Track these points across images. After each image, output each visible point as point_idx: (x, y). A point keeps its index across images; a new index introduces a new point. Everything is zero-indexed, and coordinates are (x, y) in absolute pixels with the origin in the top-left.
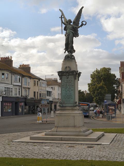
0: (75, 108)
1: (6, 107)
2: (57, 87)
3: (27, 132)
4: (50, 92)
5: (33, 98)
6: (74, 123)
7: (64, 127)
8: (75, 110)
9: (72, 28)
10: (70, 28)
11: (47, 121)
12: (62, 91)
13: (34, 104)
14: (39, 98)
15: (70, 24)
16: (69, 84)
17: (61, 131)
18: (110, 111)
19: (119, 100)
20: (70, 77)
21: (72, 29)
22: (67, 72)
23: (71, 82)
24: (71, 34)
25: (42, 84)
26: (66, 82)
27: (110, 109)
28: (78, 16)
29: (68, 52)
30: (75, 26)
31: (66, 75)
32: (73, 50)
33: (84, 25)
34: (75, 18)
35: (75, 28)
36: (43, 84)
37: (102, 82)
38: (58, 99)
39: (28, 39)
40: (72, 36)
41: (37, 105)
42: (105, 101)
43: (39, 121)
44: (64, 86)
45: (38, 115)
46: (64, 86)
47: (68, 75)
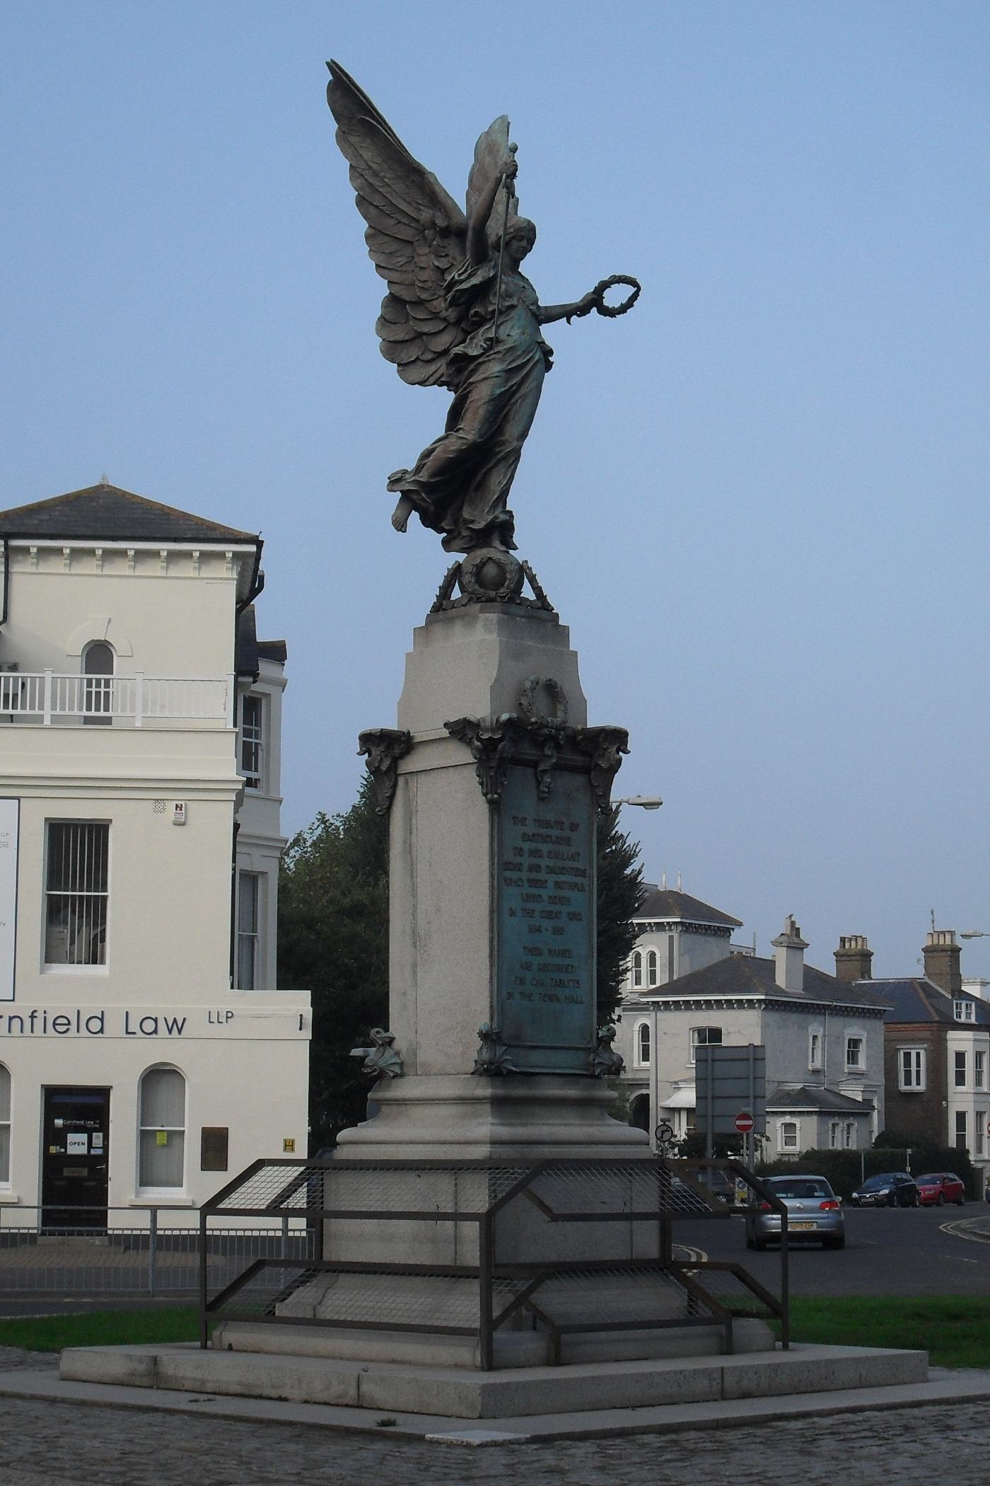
23: (567, 841)
26: (531, 829)
31: (534, 765)
39: (306, 1129)
44: (519, 867)
46: (519, 867)
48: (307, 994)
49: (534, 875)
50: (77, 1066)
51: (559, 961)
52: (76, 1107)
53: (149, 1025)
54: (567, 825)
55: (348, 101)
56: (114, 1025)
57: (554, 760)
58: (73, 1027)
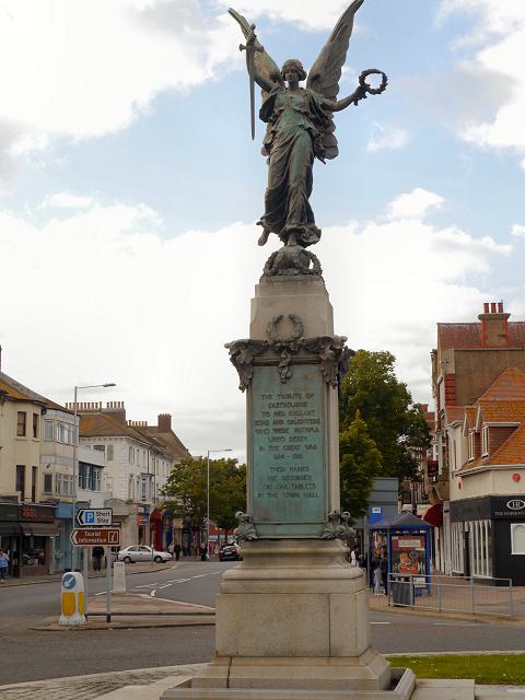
0: (330, 549)
1: (424, 579)
2: (124, 442)
3: (31, 684)
4: (93, 466)
5: (14, 498)
6: (327, 635)
7: (270, 656)
8: (331, 557)
9: (300, 111)
10: (298, 108)
11: (109, 616)
12: (257, 449)
13: (16, 525)
14: (40, 497)
15: (294, 86)
17: (251, 684)
18: (403, 559)
19: (429, 506)
20: (298, 371)
21: (306, 114)
22: (283, 348)
23: (305, 404)
24: (304, 141)
25: (58, 429)
26: (274, 401)
27: (402, 551)
28: (333, 46)
29: (284, 238)
30: (320, 99)
31: (276, 364)
32: (311, 226)
33: (374, 92)
34: (318, 61)
35: (324, 106)
36: (62, 428)
37: (358, 420)
38: (129, 502)
40: (309, 149)
41: (30, 529)
42: (376, 510)
43: (69, 614)
44: (267, 423)
45: (67, 584)
46: (267, 423)
47: (290, 364)
51: (300, 474)
54: (304, 394)
57: (288, 360)
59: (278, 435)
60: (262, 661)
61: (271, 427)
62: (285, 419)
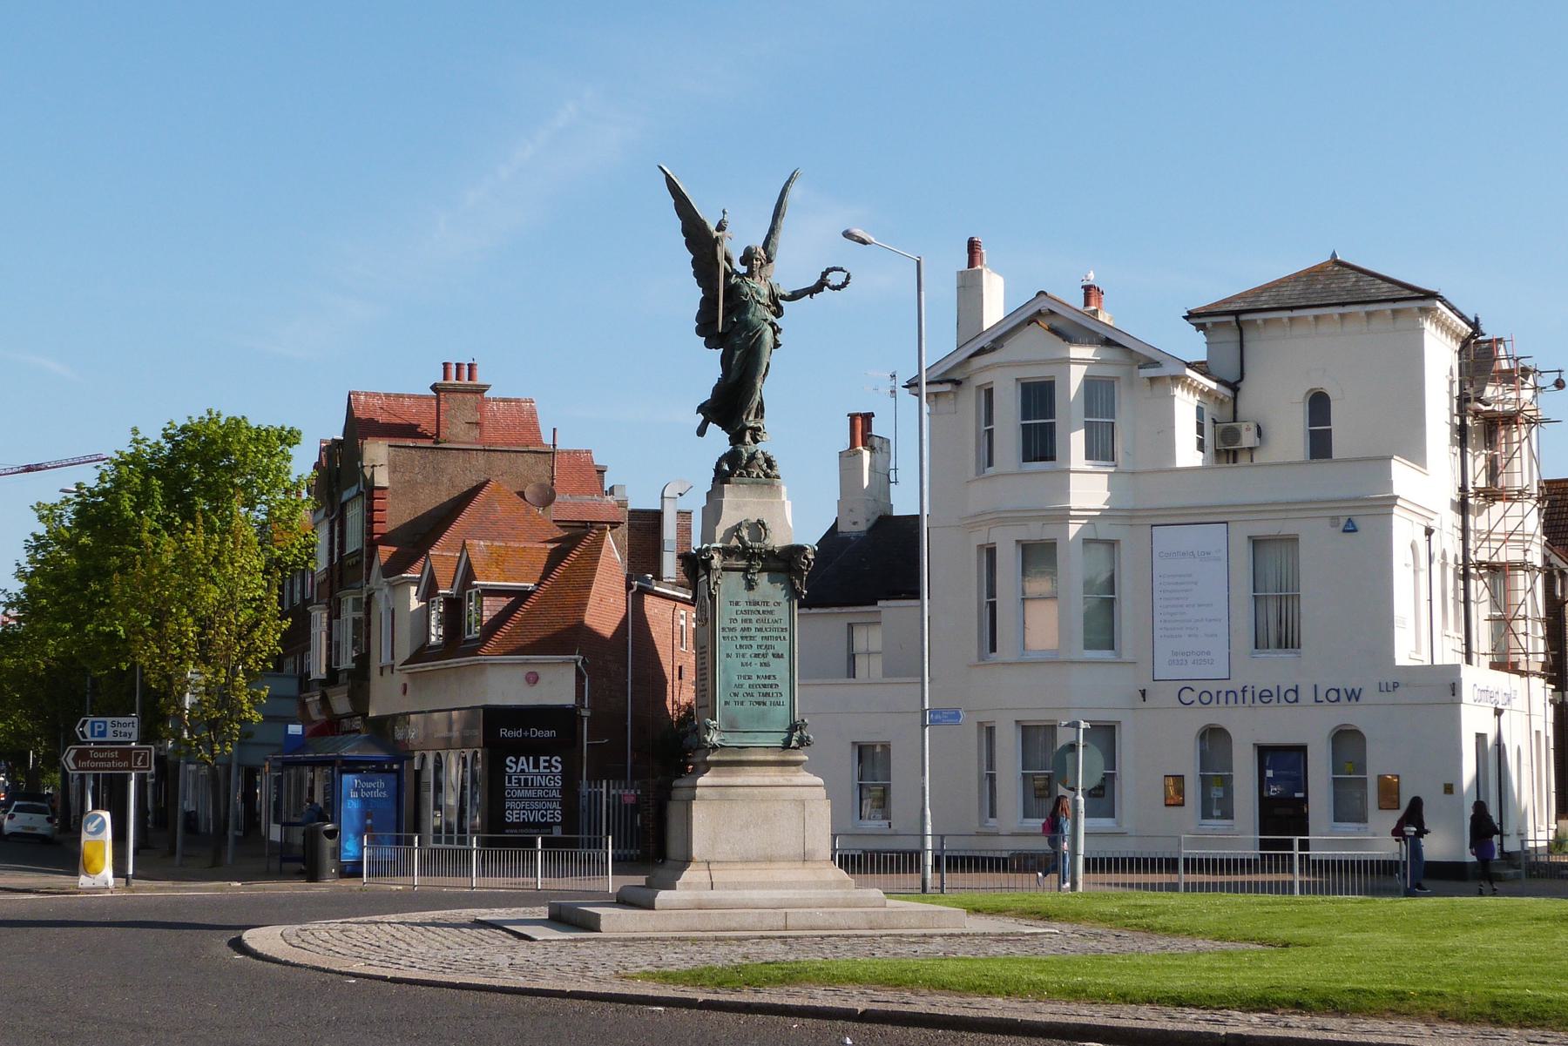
7: (747, 861)
16: (763, 621)
17: (736, 886)
23: (771, 612)
33: (834, 288)
44: (733, 629)
46: (733, 629)
48: (1398, 663)
49: (746, 634)
50: (1280, 728)
51: (767, 682)
52: (1282, 761)
53: (1333, 696)
55: (669, 180)
56: (1306, 695)
58: (1275, 698)
59: (745, 642)
60: (740, 866)
61: (738, 634)
62: (753, 626)
